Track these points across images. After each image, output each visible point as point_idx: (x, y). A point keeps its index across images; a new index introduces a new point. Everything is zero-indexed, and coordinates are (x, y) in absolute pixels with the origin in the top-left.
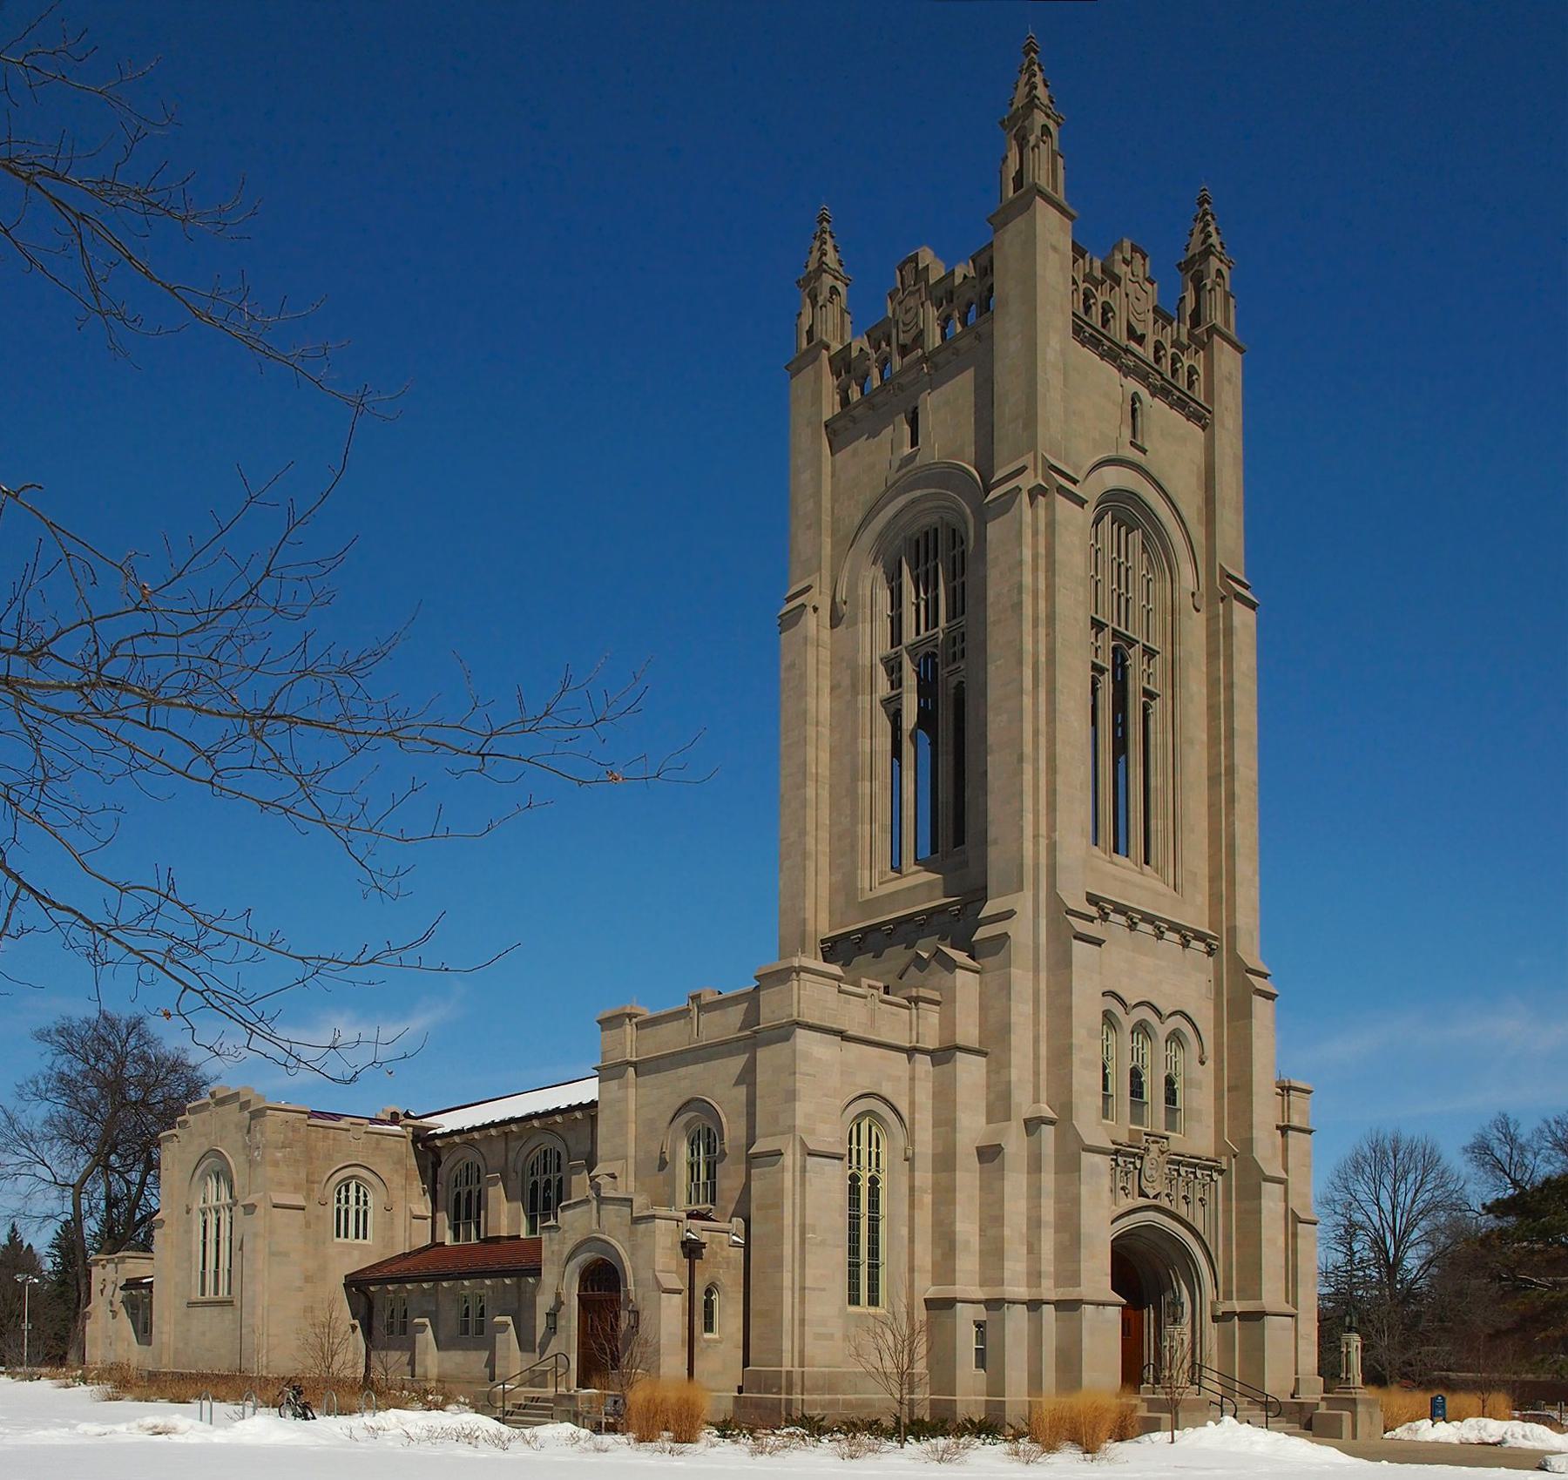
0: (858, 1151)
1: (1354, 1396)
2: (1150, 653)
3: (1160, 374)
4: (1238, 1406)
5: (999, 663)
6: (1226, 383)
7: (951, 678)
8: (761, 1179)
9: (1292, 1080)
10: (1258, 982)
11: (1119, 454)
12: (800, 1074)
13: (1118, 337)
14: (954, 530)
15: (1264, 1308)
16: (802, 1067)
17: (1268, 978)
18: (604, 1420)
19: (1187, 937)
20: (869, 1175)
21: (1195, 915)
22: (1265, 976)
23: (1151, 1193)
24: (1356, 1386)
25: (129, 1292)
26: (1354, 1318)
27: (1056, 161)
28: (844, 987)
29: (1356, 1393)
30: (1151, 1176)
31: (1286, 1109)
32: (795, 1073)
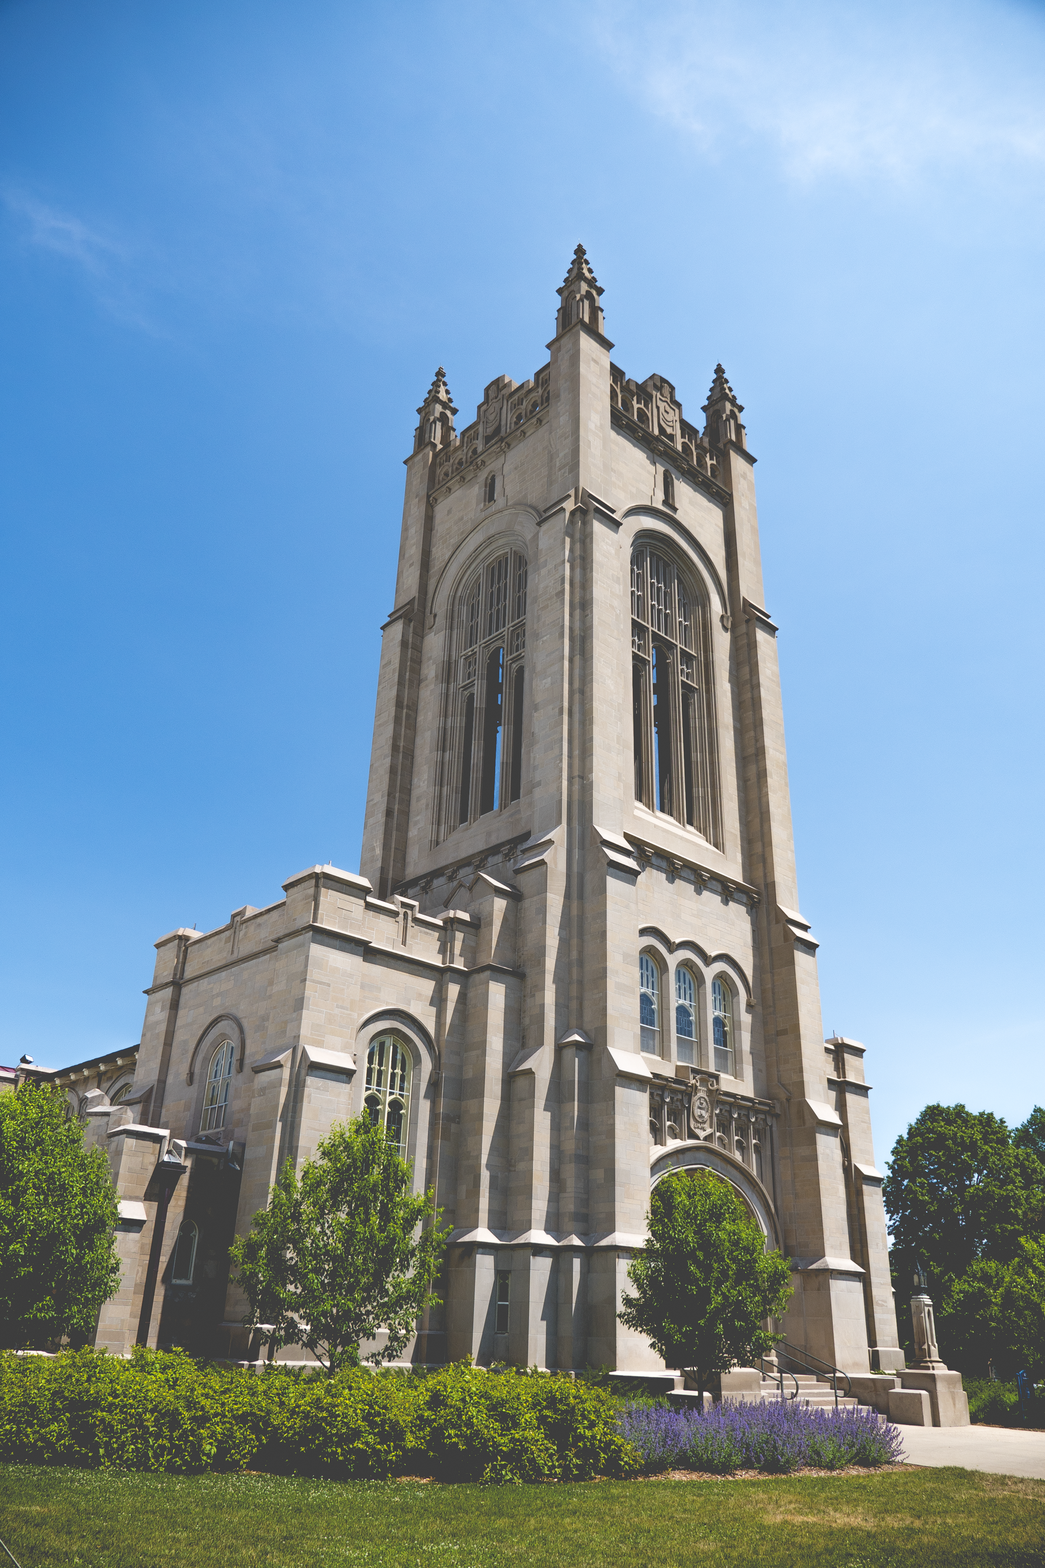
0: (380, 1072)
1: (931, 1372)
2: (687, 658)
3: (687, 461)
4: (799, 1383)
5: (545, 638)
6: (742, 479)
7: (514, 666)
8: (261, 1096)
9: (844, 1039)
10: (799, 933)
11: (653, 505)
12: (313, 981)
13: (651, 430)
14: (520, 557)
15: (827, 1265)
16: (313, 973)
17: (809, 930)
18: (427, 1332)
19: (727, 890)
20: (389, 1099)
21: (732, 869)
22: (805, 928)
23: (702, 1134)
24: (933, 1359)
25: (653, 1239)
26: (922, 1278)
27: (752, 645)
28: (370, 899)
29: (933, 1368)
30: (701, 1116)
31: (840, 1066)
32: (305, 980)
